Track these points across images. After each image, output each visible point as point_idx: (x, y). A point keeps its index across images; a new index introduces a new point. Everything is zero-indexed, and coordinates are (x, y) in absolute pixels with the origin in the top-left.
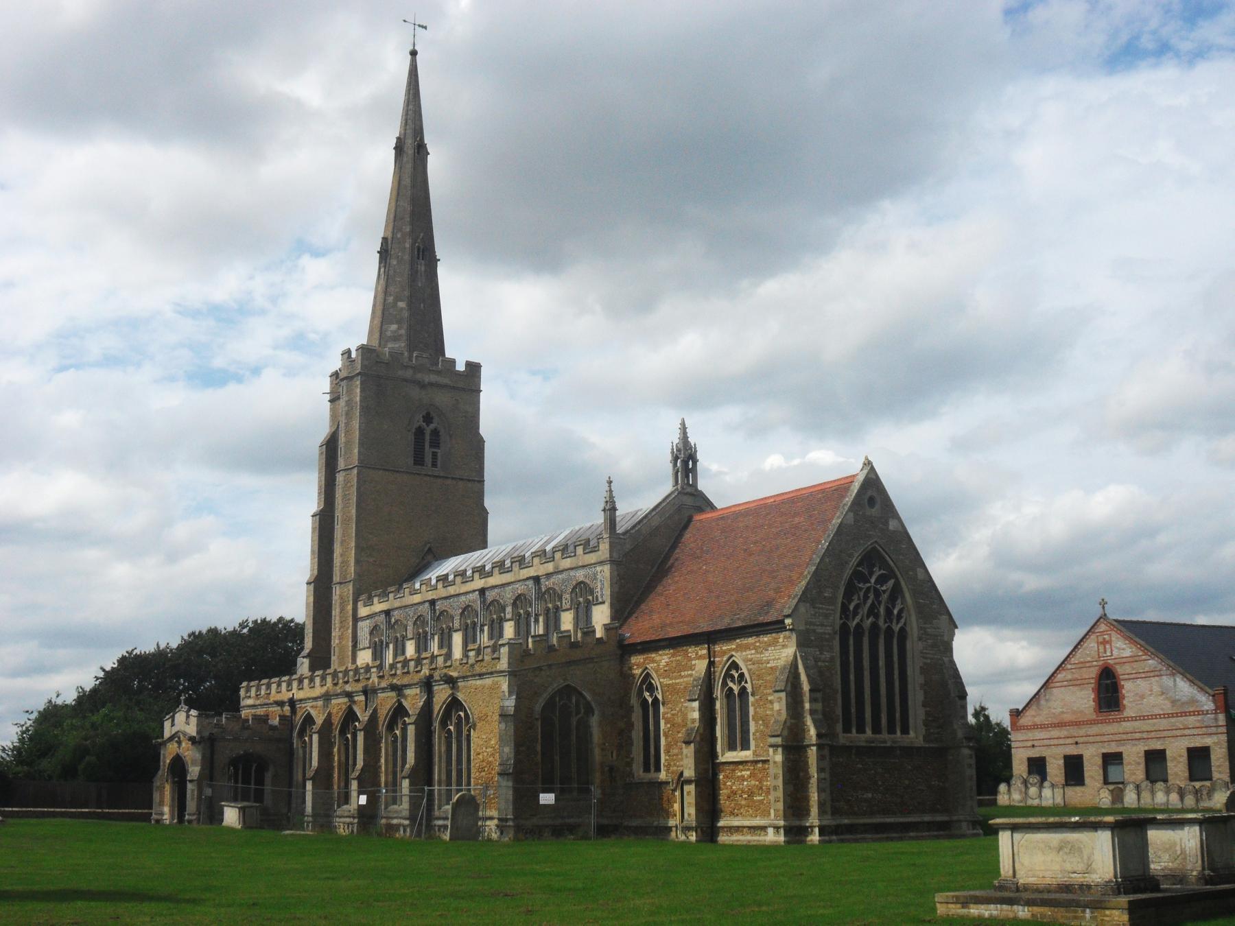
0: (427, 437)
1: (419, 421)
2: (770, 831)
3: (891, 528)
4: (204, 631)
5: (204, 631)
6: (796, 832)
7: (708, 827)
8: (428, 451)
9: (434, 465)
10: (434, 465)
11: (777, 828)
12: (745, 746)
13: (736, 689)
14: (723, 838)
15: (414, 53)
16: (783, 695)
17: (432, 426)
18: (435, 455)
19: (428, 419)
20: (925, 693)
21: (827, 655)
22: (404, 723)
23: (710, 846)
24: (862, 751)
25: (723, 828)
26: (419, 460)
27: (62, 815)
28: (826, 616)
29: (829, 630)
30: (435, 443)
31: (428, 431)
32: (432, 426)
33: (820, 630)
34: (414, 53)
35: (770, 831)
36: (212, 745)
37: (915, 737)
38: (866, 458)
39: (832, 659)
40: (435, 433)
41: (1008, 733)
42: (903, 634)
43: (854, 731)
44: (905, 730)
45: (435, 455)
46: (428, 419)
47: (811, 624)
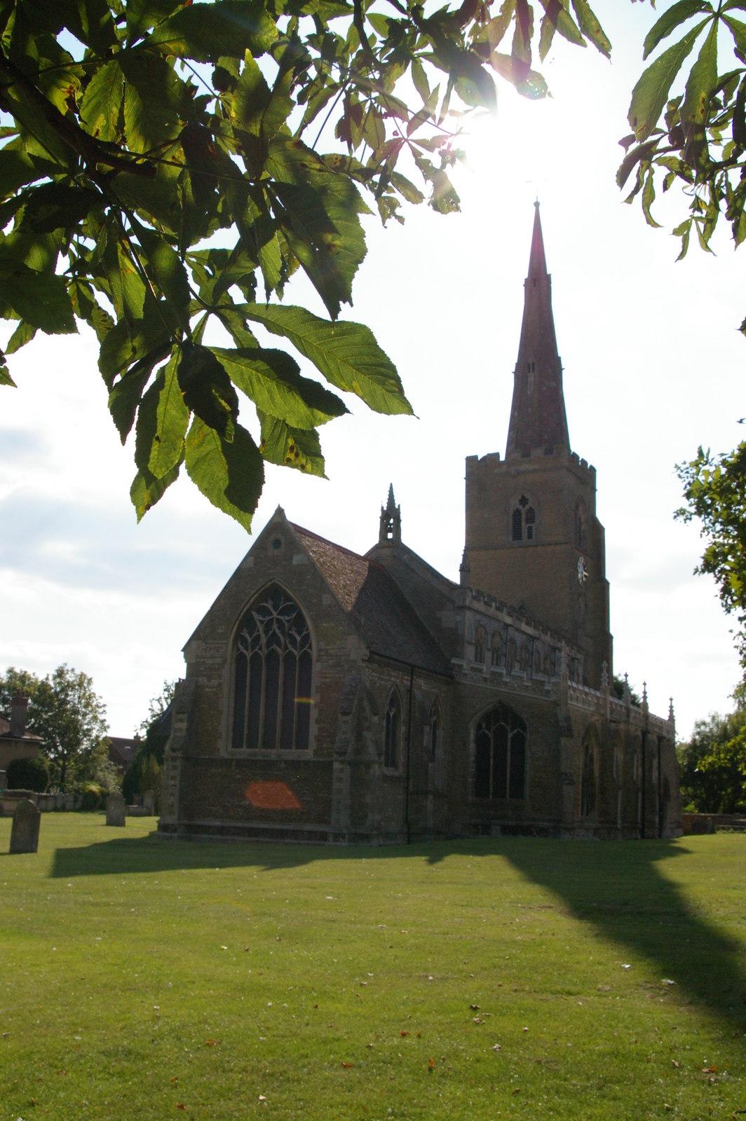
0: (524, 516)
1: (514, 503)
4: (633, 693)
5: (633, 693)
9: (530, 536)
10: (530, 536)
12: (302, 744)
13: (248, 654)
16: (185, 716)
17: (527, 507)
18: (530, 529)
19: (524, 501)
22: (391, 762)
26: (517, 535)
30: (531, 518)
31: (524, 511)
32: (527, 507)
34: (537, 204)
35: (331, 838)
37: (309, 754)
38: (664, 191)
39: (220, 685)
41: (221, 120)
43: (293, 747)
44: (302, 744)
45: (530, 529)
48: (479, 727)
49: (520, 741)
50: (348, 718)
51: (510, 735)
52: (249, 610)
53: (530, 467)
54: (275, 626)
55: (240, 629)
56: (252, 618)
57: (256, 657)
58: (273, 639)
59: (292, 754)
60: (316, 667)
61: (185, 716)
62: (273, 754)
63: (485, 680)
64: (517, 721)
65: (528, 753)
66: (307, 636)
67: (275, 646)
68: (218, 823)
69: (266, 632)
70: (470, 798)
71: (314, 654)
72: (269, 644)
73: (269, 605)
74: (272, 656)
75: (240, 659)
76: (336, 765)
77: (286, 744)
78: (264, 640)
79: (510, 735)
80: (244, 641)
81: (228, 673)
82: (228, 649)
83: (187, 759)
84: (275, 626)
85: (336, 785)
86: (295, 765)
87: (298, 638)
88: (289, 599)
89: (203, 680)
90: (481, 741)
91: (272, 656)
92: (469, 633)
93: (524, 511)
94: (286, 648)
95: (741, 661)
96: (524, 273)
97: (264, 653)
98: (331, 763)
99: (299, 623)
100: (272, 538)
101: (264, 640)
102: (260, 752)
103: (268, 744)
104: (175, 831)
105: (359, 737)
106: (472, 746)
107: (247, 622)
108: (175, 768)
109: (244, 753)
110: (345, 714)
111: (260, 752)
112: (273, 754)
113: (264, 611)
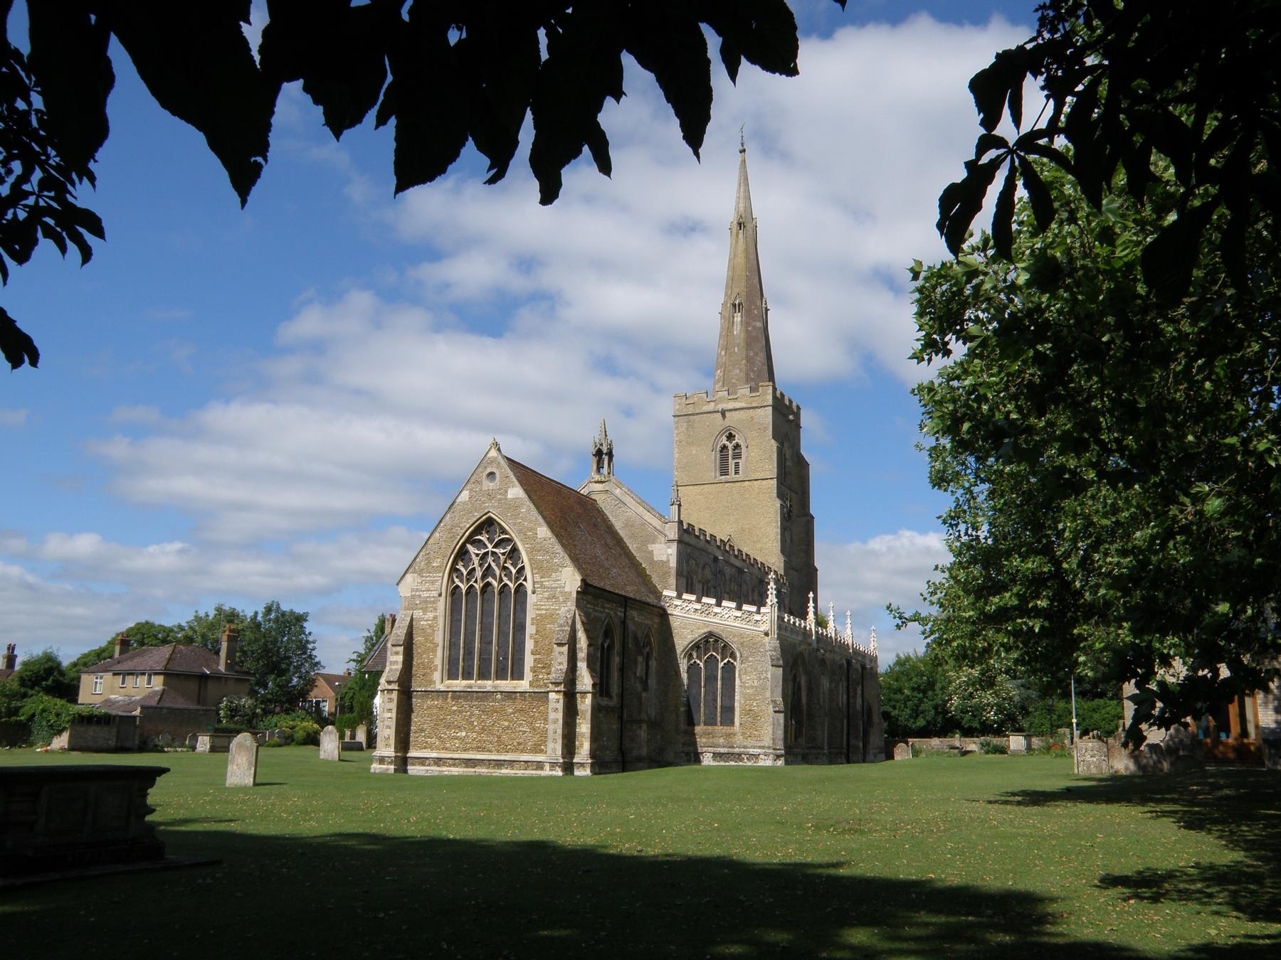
2: (547, 767)
3: (509, 496)
6: (568, 767)
7: (402, 763)
8: (731, 463)
11: (553, 765)
12: (518, 675)
13: (464, 587)
14: (413, 770)
19: (730, 437)
21: (430, 615)
23: (403, 775)
24: (457, 695)
25: (390, 763)
26: (724, 472)
27: (206, 820)
28: (433, 582)
29: (435, 594)
30: (737, 456)
31: (730, 446)
33: (425, 595)
35: (547, 767)
36: (622, 751)
37: (524, 685)
39: (435, 618)
40: (737, 446)
42: (520, 589)
44: (518, 675)
45: (737, 465)
46: (730, 437)
47: (417, 590)
49: (729, 670)
52: (464, 545)
54: (490, 559)
55: (455, 562)
56: (467, 552)
58: (488, 572)
59: (507, 685)
60: (531, 599)
61: (401, 649)
62: (488, 685)
64: (726, 650)
66: (523, 568)
67: (490, 579)
68: (434, 755)
69: (481, 565)
71: (529, 586)
72: (484, 576)
73: (484, 538)
76: (552, 696)
77: (501, 675)
78: (479, 573)
80: (460, 576)
81: (442, 605)
86: (510, 695)
87: (514, 571)
88: (504, 531)
93: (730, 446)
94: (501, 580)
99: (514, 554)
102: (476, 684)
103: (484, 675)
107: (462, 554)
110: (560, 645)
113: (479, 544)
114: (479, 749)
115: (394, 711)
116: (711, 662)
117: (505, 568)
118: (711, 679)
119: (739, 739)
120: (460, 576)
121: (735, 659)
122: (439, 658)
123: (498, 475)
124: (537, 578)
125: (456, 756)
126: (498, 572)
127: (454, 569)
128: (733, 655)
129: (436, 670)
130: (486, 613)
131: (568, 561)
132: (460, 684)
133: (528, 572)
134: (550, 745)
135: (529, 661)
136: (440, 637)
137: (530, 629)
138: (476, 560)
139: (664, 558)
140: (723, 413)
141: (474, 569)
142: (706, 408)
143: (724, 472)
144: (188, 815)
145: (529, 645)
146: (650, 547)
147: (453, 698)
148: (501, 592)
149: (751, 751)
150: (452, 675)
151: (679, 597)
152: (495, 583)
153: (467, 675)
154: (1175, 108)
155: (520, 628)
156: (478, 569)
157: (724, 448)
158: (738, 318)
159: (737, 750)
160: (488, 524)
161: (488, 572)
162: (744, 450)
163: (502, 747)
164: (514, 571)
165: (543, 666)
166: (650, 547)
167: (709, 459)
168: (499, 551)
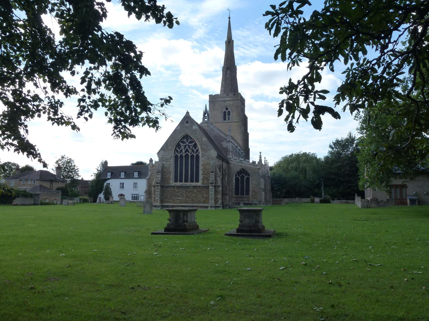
3: (193, 128)
8: (227, 116)
9: (229, 120)
10: (229, 120)
12: (197, 181)
13: (179, 155)
15: (229, 18)
16: (160, 173)
18: (229, 117)
19: (227, 109)
20: (203, 171)
24: (178, 187)
26: (225, 119)
27: (175, 234)
28: (169, 154)
29: (170, 157)
30: (229, 114)
31: (227, 112)
33: (166, 157)
34: (229, 18)
35: (209, 207)
37: (199, 184)
39: (170, 164)
40: (229, 112)
42: (198, 156)
44: (197, 181)
45: (229, 117)
46: (227, 109)
48: (236, 175)
49: (248, 179)
50: (213, 174)
51: (245, 178)
52: (179, 142)
53: (229, 99)
54: (187, 147)
55: (176, 148)
56: (180, 145)
57: (181, 156)
58: (187, 151)
59: (194, 184)
60: (201, 159)
61: (160, 173)
62: (188, 184)
63: (238, 162)
64: (247, 174)
65: (250, 183)
66: (198, 150)
67: (187, 153)
68: (171, 204)
69: (184, 149)
70: (234, 196)
71: (200, 155)
72: (185, 152)
73: (185, 140)
74: (187, 156)
75: (176, 157)
76: (210, 187)
77: (192, 181)
78: (184, 151)
79: (245, 178)
80: (177, 152)
81: (172, 161)
82: (172, 154)
83: (161, 186)
84: (187, 147)
85: (210, 193)
86: (195, 187)
87: (195, 151)
88: (191, 138)
89: (164, 163)
90: (237, 179)
91: (187, 156)
92: (230, 148)
93: (227, 112)
94: (191, 153)
95: (15, 150)
96: (226, 39)
97: (184, 155)
98: (209, 186)
99: (195, 146)
100: (186, 120)
101: (184, 151)
102: (183, 184)
103: (186, 181)
104: (159, 207)
105: (216, 179)
106: (234, 181)
107: (178, 145)
108: (158, 189)
109: (179, 184)
110: (212, 172)
111: (183, 184)
112: (188, 184)
113: (183, 142)
114: (185, 203)
115: (159, 191)
116: (243, 177)
117: (192, 150)
118: (242, 182)
119: (251, 199)
120: (177, 152)
121: (249, 176)
122: (172, 176)
123: (189, 122)
124: (203, 153)
125: (178, 205)
126: (190, 151)
127: (176, 150)
128: (249, 176)
129: (171, 179)
130: (187, 163)
131: (213, 148)
132: (179, 184)
133: (200, 151)
134: (210, 201)
135: (201, 177)
136: (172, 169)
137: (201, 168)
138: (183, 147)
139: (226, 147)
140: (225, 101)
141: (182, 150)
142: (219, 100)
143: (225, 119)
144: (232, 237)
145: (201, 172)
146: (222, 143)
147: (177, 188)
148: (191, 157)
149: (255, 202)
150: (176, 181)
151: (245, 160)
152: (189, 154)
153: (181, 181)
154: (424, 44)
155: (198, 167)
156: (183, 148)
157: (225, 112)
158: (228, 72)
159: (250, 202)
160: (186, 137)
161: (187, 151)
162: (231, 113)
163: (193, 202)
164: (195, 151)
165: (206, 178)
166: (222, 143)
167: (221, 115)
168: (190, 144)
